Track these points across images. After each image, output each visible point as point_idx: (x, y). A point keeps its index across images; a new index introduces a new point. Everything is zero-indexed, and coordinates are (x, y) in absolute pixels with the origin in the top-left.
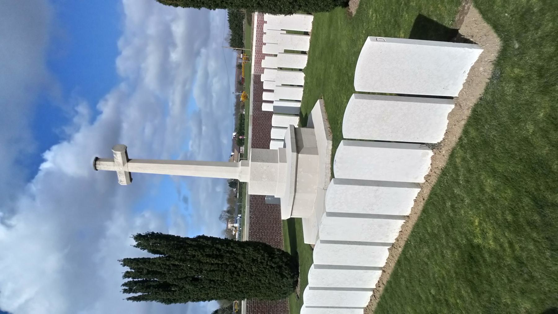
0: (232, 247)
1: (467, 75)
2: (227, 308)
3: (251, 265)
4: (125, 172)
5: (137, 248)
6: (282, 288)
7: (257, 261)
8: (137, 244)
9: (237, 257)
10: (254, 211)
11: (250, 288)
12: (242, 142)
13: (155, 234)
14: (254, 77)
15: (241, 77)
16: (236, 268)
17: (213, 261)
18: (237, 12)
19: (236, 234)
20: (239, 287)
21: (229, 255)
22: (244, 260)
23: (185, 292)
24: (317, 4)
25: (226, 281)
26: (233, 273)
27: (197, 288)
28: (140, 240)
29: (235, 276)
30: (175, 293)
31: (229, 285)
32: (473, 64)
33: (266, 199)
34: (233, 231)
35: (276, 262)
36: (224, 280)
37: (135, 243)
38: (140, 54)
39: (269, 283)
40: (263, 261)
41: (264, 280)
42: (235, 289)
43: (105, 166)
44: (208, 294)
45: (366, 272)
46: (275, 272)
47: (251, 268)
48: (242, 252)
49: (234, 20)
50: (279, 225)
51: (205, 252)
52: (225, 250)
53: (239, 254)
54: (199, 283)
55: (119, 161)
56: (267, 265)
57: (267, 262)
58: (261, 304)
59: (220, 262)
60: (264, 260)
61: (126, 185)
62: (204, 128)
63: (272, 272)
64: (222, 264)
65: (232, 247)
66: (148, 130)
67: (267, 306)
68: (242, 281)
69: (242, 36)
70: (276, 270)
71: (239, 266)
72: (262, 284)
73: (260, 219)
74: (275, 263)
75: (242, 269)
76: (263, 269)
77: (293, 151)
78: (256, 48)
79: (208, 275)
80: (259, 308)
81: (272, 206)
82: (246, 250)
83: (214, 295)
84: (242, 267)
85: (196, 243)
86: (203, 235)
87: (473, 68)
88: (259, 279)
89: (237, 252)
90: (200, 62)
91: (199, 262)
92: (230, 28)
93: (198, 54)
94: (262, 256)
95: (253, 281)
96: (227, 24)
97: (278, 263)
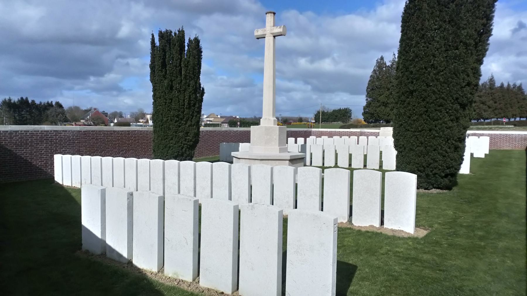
0: (196, 116)
1: (397, 229)
2: (65, 116)
3: (184, 132)
4: (266, 34)
5: (188, 41)
6: (166, 157)
7: (187, 136)
8: (191, 40)
9: (189, 120)
10: (208, 134)
11: (165, 131)
12: (232, 125)
13: (201, 54)
14: (309, 131)
15: (291, 122)
16: (182, 119)
17: (187, 101)
18: (348, 116)
19: (140, 123)
20: (166, 123)
21: (191, 114)
22: (187, 125)
23: (162, 80)
24: (403, 163)
25: (171, 112)
26: (178, 117)
27: (166, 89)
28: (195, 42)
29: (175, 119)
30: (160, 72)
31: (168, 114)
32: (405, 231)
33: (224, 143)
34: (143, 120)
35: (186, 151)
36: (172, 110)
37: (192, 38)
38: (303, 31)
39: (170, 147)
40: (187, 141)
41: (173, 142)
42: (165, 119)
43: (270, 20)
44: (160, 98)
45: (247, 200)
46: (179, 151)
47: (181, 132)
48: (193, 123)
49: (341, 114)
50: (197, 155)
51: (192, 94)
52: (194, 110)
53: (192, 122)
54: (169, 91)
55: (274, 30)
56: (184, 144)
57: (186, 144)
58: (137, 143)
59: (186, 106)
60: (188, 142)
61: (255, 35)
62: (239, 89)
63: (179, 148)
64: (184, 108)
65: (196, 116)
66: (234, 39)
67: (136, 147)
68: (171, 125)
69: (327, 122)
70: (180, 151)
71: (183, 122)
72: (169, 141)
73: (202, 139)
74: (185, 151)
75: (181, 124)
76: (181, 142)
77: (291, 156)
78: (333, 131)
79: (175, 98)
80: (135, 141)
81: (211, 149)
82: (195, 127)
83: (159, 103)
84: (182, 124)
85: (198, 87)
86: (205, 93)
87: (403, 231)
88: (173, 138)
89: (193, 119)
90: (299, 85)
91: (185, 90)
92: (334, 111)
93: (306, 83)
94: (191, 140)
95: (171, 134)
96: (337, 108)
97: (186, 153)
